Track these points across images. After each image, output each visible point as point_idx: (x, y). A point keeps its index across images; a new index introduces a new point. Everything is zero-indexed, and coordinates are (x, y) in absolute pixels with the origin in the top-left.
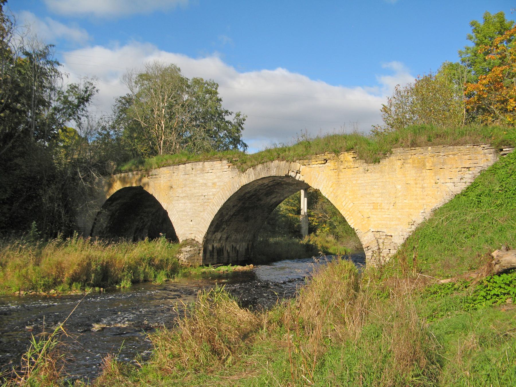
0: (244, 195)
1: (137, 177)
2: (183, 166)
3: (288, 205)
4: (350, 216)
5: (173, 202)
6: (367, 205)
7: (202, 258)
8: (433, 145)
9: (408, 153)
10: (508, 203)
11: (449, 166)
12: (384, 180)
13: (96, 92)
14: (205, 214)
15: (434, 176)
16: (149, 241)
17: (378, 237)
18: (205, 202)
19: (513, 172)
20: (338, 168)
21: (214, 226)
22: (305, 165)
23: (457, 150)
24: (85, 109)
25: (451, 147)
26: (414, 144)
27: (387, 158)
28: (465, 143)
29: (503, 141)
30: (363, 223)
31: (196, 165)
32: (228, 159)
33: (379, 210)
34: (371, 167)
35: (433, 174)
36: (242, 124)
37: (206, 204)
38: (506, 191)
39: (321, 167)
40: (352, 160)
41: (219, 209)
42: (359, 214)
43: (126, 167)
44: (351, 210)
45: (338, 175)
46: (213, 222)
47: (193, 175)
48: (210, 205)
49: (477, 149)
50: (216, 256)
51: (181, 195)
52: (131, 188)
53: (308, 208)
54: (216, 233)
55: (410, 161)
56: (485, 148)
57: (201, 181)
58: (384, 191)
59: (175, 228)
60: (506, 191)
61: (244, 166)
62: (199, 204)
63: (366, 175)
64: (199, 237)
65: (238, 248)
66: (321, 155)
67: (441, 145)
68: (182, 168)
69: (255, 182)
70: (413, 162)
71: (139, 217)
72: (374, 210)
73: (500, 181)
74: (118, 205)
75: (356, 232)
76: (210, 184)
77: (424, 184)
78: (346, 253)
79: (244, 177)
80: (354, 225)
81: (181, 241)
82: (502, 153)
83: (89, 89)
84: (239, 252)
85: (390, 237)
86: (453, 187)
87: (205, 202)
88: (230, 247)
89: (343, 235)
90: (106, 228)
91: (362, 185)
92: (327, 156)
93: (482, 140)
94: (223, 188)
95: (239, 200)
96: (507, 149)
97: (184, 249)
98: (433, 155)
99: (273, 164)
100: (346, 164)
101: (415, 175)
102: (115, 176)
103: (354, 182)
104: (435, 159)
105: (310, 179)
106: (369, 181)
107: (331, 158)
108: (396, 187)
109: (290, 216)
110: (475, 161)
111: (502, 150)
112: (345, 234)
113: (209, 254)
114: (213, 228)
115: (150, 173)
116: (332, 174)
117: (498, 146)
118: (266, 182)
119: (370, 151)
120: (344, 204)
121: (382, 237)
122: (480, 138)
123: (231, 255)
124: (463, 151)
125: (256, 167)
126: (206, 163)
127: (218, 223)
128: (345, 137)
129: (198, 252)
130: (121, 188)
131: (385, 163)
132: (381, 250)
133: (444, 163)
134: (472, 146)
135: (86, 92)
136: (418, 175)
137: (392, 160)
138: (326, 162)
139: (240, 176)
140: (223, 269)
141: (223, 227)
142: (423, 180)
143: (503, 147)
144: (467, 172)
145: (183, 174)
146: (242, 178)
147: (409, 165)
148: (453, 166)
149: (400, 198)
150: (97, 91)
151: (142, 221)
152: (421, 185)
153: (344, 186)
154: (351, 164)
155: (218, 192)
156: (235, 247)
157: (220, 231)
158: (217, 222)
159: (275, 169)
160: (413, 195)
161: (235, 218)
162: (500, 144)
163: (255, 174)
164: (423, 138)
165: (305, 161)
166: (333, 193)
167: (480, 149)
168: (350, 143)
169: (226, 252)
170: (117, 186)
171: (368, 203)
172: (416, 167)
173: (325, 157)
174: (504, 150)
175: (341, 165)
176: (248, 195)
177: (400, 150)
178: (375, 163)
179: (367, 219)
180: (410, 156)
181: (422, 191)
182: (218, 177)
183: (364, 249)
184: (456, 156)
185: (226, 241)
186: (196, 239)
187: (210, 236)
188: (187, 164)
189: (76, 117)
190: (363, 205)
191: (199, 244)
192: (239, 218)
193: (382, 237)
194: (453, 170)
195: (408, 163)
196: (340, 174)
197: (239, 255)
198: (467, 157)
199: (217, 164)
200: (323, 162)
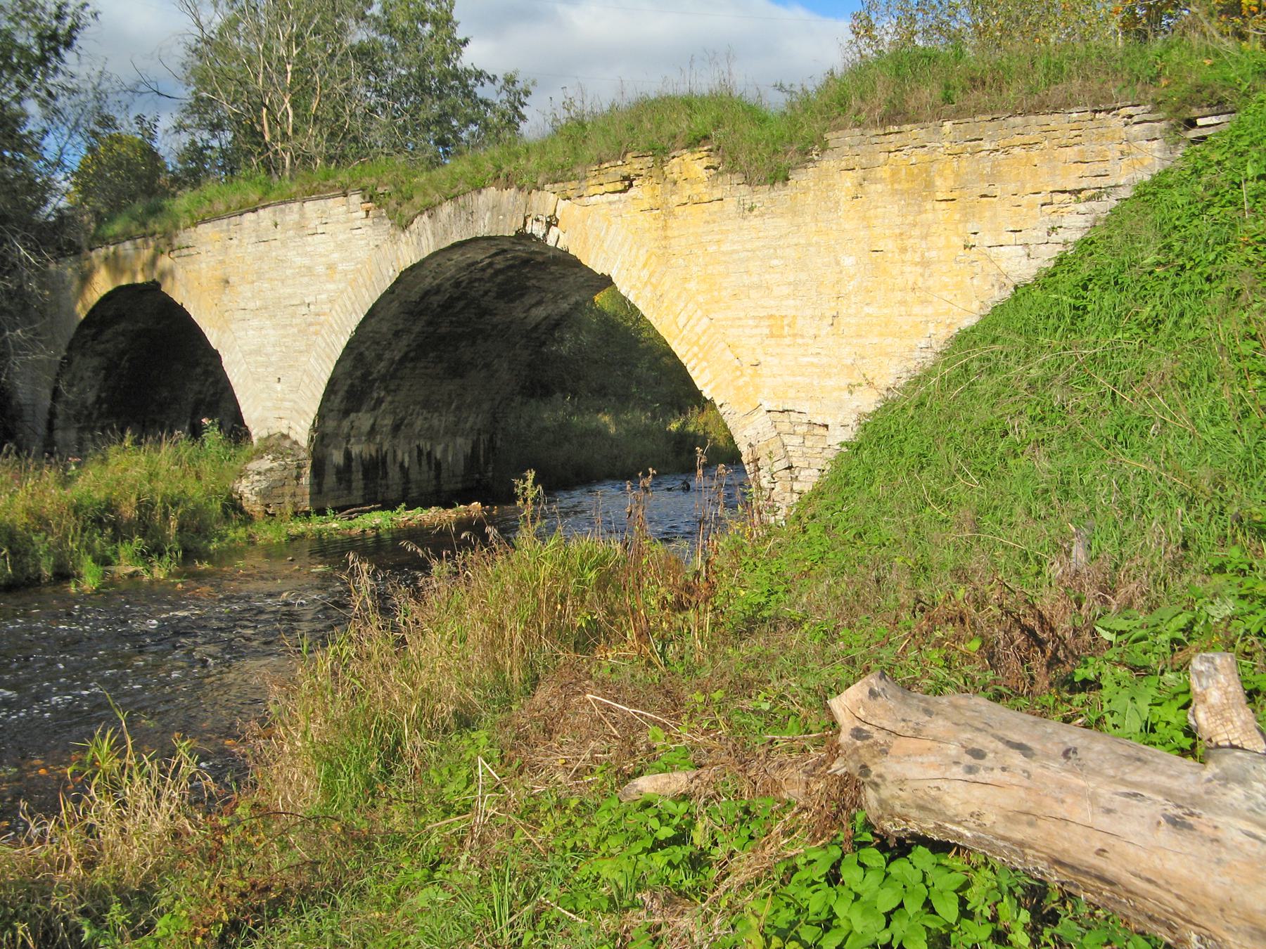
0: (422, 298)
1: (147, 254)
2: (250, 217)
5: (233, 327)
6: (751, 322)
7: (308, 490)
8: (959, 113)
9: (878, 147)
10: (1182, 315)
11: (1012, 187)
12: (803, 241)
13: (91, 20)
14: (312, 360)
15: (960, 221)
16: (137, 443)
17: (785, 427)
18: (310, 324)
19: (1217, 194)
20: (666, 203)
21: (341, 394)
22: (569, 199)
23: (1039, 129)
24: (62, 67)
25: (1019, 120)
26: (896, 115)
27: (811, 164)
28: (1065, 105)
29: (1199, 89)
30: (741, 381)
31: (283, 211)
32: (363, 189)
33: (787, 341)
34: (763, 196)
35: (957, 217)
36: (523, 104)
37: (312, 329)
38: (1183, 267)
39: (614, 202)
40: (704, 174)
41: (344, 343)
42: (728, 352)
43: (117, 228)
44: (704, 339)
45: (665, 228)
47: (278, 243)
48: (323, 332)
49: (1106, 123)
51: (251, 305)
52: (133, 287)
54: (353, 416)
55: (884, 172)
56: (1136, 119)
57: (299, 261)
58: (803, 276)
59: (241, 402)
60: (1183, 267)
61: (407, 210)
62: (295, 330)
63: (746, 223)
64: (298, 429)
65: (439, 456)
66: (613, 163)
67: (984, 112)
68: (251, 222)
69: (439, 259)
70: (893, 175)
71: (199, 370)
72: (773, 341)
73: (1166, 228)
74: (121, 338)
75: (721, 411)
76: (321, 269)
77: (929, 249)
79: (407, 243)
81: (255, 439)
82: (1193, 134)
83: (69, 10)
84: (444, 466)
85: (822, 431)
86: (1024, 260)
87: (310, 324)
88: (410, 453)
90: (99, 400)
91: (735, 256)
92: (634, 165)
93: (1125, 92)
94: (355, 280)
95: (411, 313)
96: (1213, 120)
97: (254, 465)
98: (957, 149)
99: (481, 198)
100: (687, 190)
101: (899, 220)
102: (93, 254)
103: (712, 249)
104: (964, 163)
105: (585, 243)
106: (757, 244)
107: (643, 172)
108: (838, 263)
110: (1099, 168)
111: (1191, 124)
113: (334, 478)
114: (337, 401)
115: (176, 242)
116: (647, 226)
117: (1177, 110)
118: (478, 255)
119: (758, 142)
120: (682, 320)
121: (800, 430)
122: (1120, 84)
123: (414, 475)
124: (1058, 134)
125: (438, 210)
126: (308, 204)
127: (352, 386)
128: (689, 104)
129: (295, 474)
130: (110, 288)
131: (804, 183)
132: (796, 472)
133: (993, 179)
134: (1088, 115)
135: (59, 17)
136: (910, 219)
137: (827, 170)
138: (631, 185)
139: (394, 240)
140: (376, 520)
141: (375, 395)
142: (925, 237)
143: (1195, 112)
144: (1072, 207)
145: (254, 239)
146: (403, 247)
147: (879, 187)
148: (1023, 186)
149: (853, 299)
150: (95, 15)
151: (211, 380)
152: (919, 254)
153: (681, 261)
154: (701, 188)
155: (342, 292)
156: (429, 454)
157: (365, 408)
158: (349, 382)
159: (488, 214)
160: (893, 290)
161: (414, 368)
162: (1187, 102)
163: (434, 234)
164: (929, 93)
165: (569, 186)
166: (649, 288)
167: (1115, 122)
168: (701, 122)
170: (102, 284)
171: (754, 318)
172: (902, 193)
173: (626, 170)
174: (1200, 122)
175: (673, 193)
176: (436, 300)
177: (849, 136)
178: (773, 184)
179: (750, 371)
180: (883, 156)
181: (922, 275)
182: (340, 246)
184: (1034, 153)
185: (394, 437)
186: (293, 436)
187: (331, 424)
188: (261, 212)
189: (43, 94)
191: (300, 447)
192: (426, 368)
193: (800, 430)
194: (1024, 202)
195: (875, 181)
196: (671, 222)
197: (444, 475)
198: (1071, 153)
199: (336, 206)
200: (620, 186)
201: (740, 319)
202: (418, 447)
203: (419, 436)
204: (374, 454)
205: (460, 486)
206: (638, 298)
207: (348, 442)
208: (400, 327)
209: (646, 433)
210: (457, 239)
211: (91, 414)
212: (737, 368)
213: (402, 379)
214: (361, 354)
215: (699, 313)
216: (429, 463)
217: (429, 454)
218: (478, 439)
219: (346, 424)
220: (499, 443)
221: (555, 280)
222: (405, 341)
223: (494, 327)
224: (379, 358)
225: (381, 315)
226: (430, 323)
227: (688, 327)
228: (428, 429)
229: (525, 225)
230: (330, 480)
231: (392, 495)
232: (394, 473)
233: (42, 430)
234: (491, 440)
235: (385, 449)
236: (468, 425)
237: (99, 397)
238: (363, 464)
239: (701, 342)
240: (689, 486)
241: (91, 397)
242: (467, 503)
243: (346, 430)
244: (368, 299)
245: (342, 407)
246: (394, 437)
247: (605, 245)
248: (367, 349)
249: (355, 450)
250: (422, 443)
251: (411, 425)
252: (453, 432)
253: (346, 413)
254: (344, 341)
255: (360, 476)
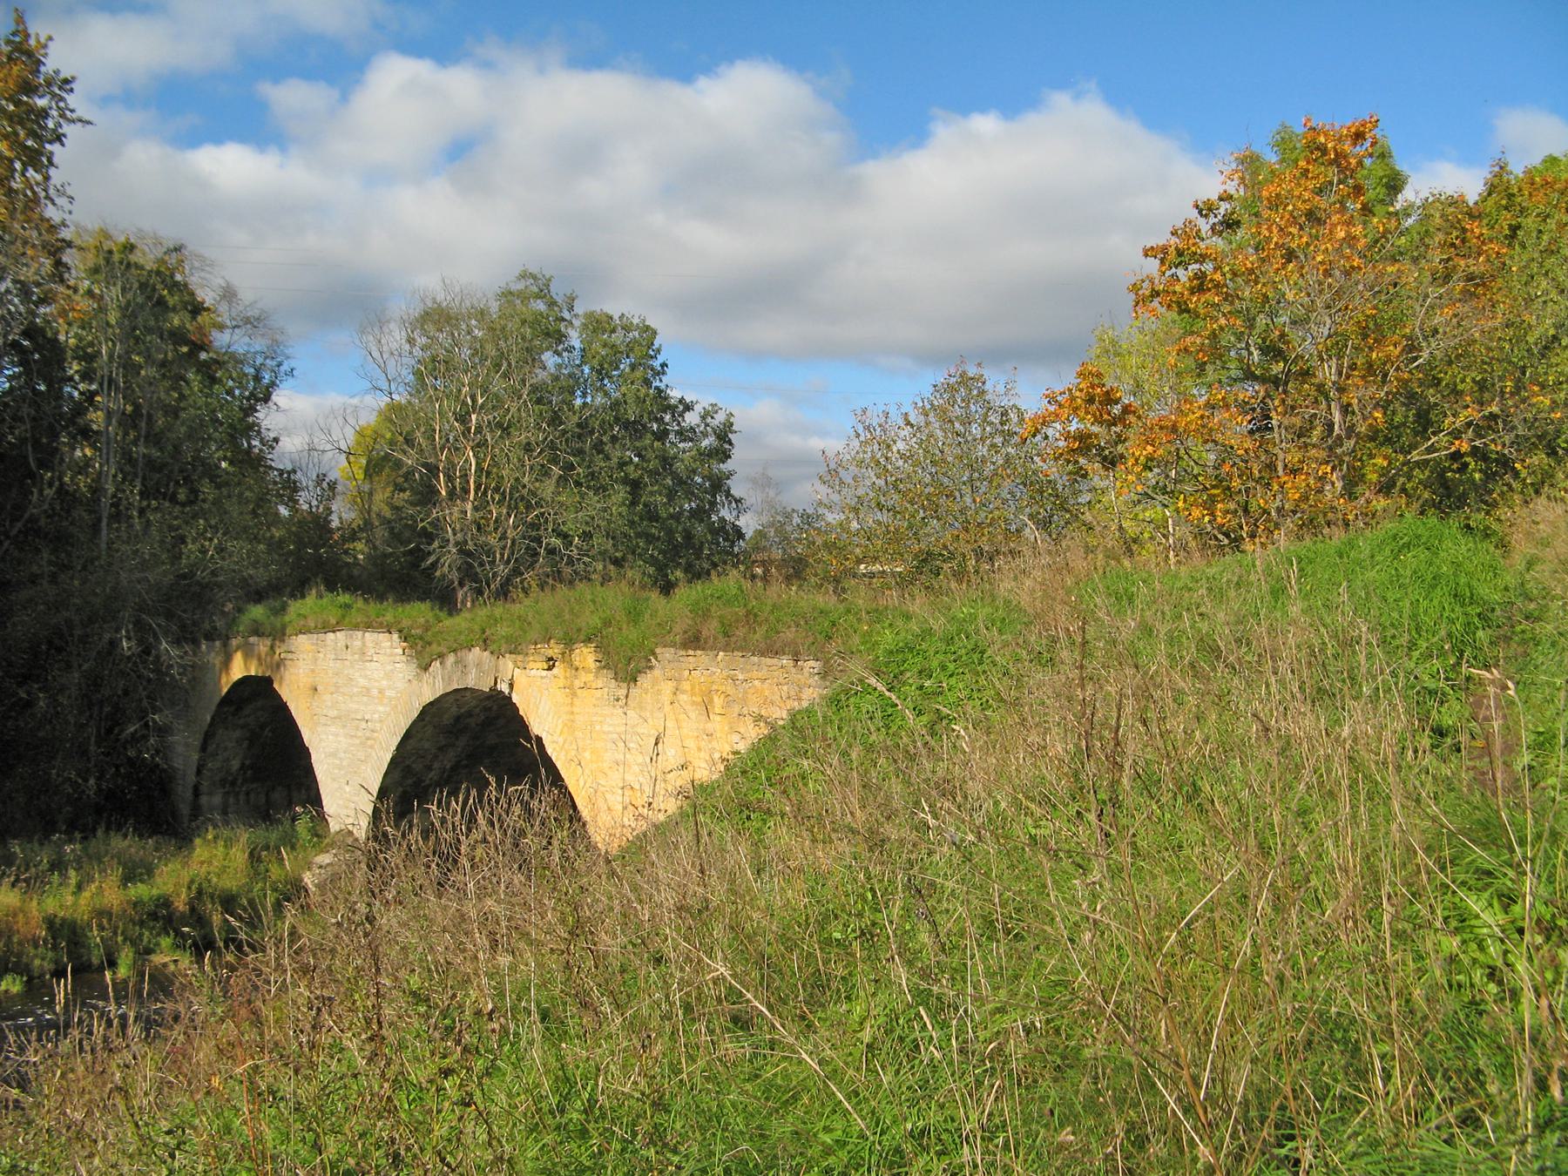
2: (331, 636)
18: (368, 739)
37: (369, 742)
57: (362, 682)
76: (375, 692)
87: (368, 739)
90: (243, 767)
92: (555, 650)
126: (367, 634)
127: (405, 792)
154: (591, 677)
158: (401, 789)
166: (563, 753)
173: (550, 653)
176: (472, 722)
210: (456, 687)
211: (236, 779)
224: (429, 768)
233: (189, 794)
237: (243, 764)
241: (235, 764)
244: (404, 724)
254: (389, 757)
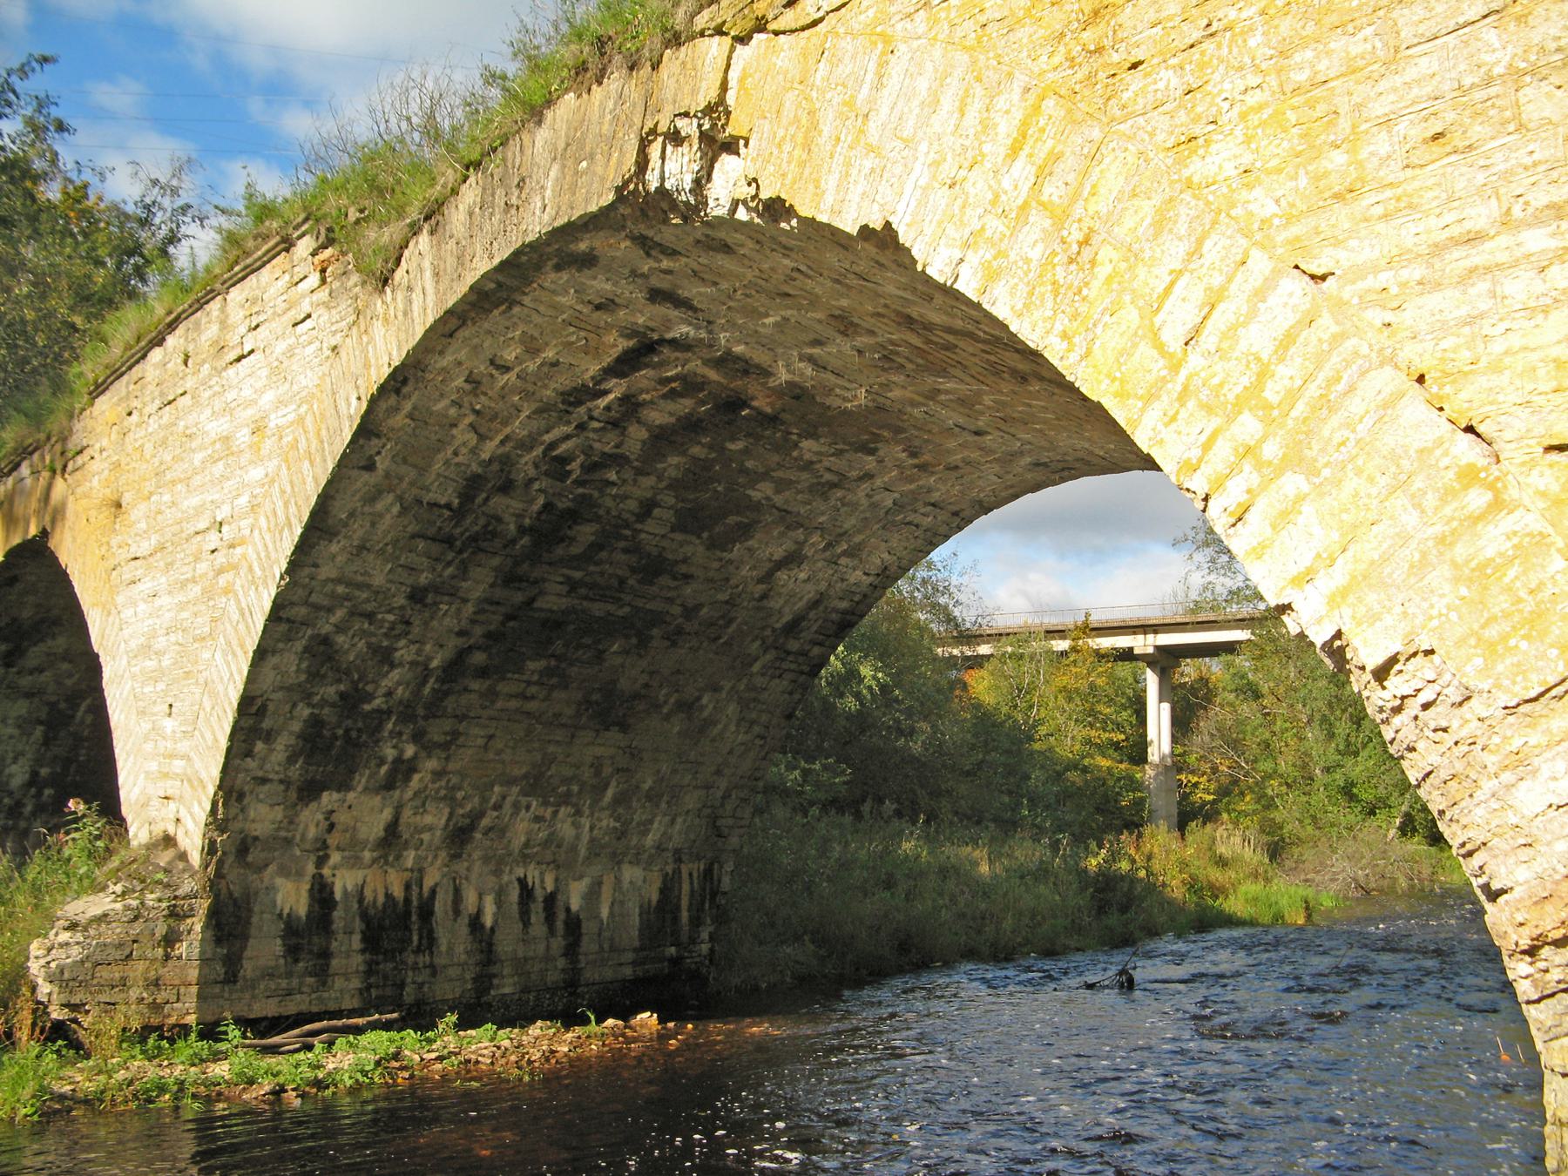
3: (1091, 725)
4: (1280, 469)
7: (193, 974)
30: (1493, 540)
42: (1415, 407)
44: (1285, 375)
46: (251, 709)
50: (358, 961)
53: (1175, 740)
54: (328, 798)
65: (575, 904)
69: (457, 353)
75: (1377, 698)
78: (1309, 917)
80: (1338, 598)
84: (588, 927)
89: (1303, 835)
90: (34, 780)
94: (294, 445)
109: (1099, 768)
112: (1309, 828)
113: (278, 947)
114: (275, 755)
120: (1176, 320)
123: (507, 944)
127: (315, 723)
129: (161, 929)
156: (550, 900)
157: (361, 780)
158: (304, 712)
161: (492, 695)
166: (1039, 222)
169: (463, 927)
176: (507, 507)
183: (1518, 969)
190: (1460, 260)
197: (588, 945)
201: (1473, 239)
202: (522, 882)
203: (525, 858)
204: (398, 892)
205: (628, 972)
206: (991, 275)
207: (321, 861)
208: (424, 579)
209: (1042, 873)
211: (19, 804)
212: (1469, 476)
213: (461, 718)
214: (325, 641)
215: (1260, 264)
216: (550, 918)
217: (550, 900)
218: (678, 871)
219: (310, 819)
220: (726, 880)
221: (823, 489)
222: (448, 619)
223: (690, 612)
224: (385, 657)
225: (358, 530)
226: (510, 579)
227: (1208, 340)
228: (546, 843)
229: (642, 164)
230: (264, 949)
231: (446, 989)
232: (453, 941)
234: (708, 873)
235: (428, 883)
236: (650, 840)
238: (364, 915)
239: (1272, 392)
240: (1131, 981)
242: (626, 1014)
243: (312, 832)
245: (295, 772)
246: (456, 857)
247: (873, 127)
248: (339, 629)
249: (343, 882)
250: (532, 874)
251: (498, 831)
252: (614, 851)
253: (309, 791)
255: (356, 941)
